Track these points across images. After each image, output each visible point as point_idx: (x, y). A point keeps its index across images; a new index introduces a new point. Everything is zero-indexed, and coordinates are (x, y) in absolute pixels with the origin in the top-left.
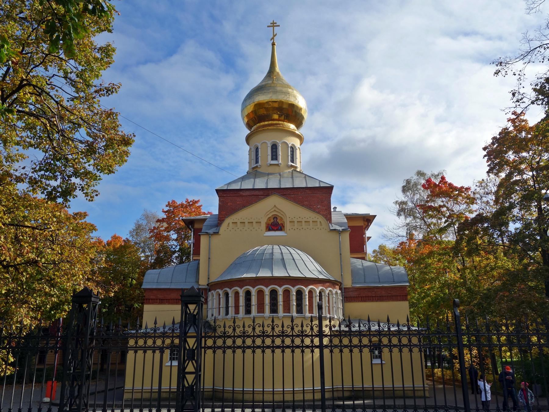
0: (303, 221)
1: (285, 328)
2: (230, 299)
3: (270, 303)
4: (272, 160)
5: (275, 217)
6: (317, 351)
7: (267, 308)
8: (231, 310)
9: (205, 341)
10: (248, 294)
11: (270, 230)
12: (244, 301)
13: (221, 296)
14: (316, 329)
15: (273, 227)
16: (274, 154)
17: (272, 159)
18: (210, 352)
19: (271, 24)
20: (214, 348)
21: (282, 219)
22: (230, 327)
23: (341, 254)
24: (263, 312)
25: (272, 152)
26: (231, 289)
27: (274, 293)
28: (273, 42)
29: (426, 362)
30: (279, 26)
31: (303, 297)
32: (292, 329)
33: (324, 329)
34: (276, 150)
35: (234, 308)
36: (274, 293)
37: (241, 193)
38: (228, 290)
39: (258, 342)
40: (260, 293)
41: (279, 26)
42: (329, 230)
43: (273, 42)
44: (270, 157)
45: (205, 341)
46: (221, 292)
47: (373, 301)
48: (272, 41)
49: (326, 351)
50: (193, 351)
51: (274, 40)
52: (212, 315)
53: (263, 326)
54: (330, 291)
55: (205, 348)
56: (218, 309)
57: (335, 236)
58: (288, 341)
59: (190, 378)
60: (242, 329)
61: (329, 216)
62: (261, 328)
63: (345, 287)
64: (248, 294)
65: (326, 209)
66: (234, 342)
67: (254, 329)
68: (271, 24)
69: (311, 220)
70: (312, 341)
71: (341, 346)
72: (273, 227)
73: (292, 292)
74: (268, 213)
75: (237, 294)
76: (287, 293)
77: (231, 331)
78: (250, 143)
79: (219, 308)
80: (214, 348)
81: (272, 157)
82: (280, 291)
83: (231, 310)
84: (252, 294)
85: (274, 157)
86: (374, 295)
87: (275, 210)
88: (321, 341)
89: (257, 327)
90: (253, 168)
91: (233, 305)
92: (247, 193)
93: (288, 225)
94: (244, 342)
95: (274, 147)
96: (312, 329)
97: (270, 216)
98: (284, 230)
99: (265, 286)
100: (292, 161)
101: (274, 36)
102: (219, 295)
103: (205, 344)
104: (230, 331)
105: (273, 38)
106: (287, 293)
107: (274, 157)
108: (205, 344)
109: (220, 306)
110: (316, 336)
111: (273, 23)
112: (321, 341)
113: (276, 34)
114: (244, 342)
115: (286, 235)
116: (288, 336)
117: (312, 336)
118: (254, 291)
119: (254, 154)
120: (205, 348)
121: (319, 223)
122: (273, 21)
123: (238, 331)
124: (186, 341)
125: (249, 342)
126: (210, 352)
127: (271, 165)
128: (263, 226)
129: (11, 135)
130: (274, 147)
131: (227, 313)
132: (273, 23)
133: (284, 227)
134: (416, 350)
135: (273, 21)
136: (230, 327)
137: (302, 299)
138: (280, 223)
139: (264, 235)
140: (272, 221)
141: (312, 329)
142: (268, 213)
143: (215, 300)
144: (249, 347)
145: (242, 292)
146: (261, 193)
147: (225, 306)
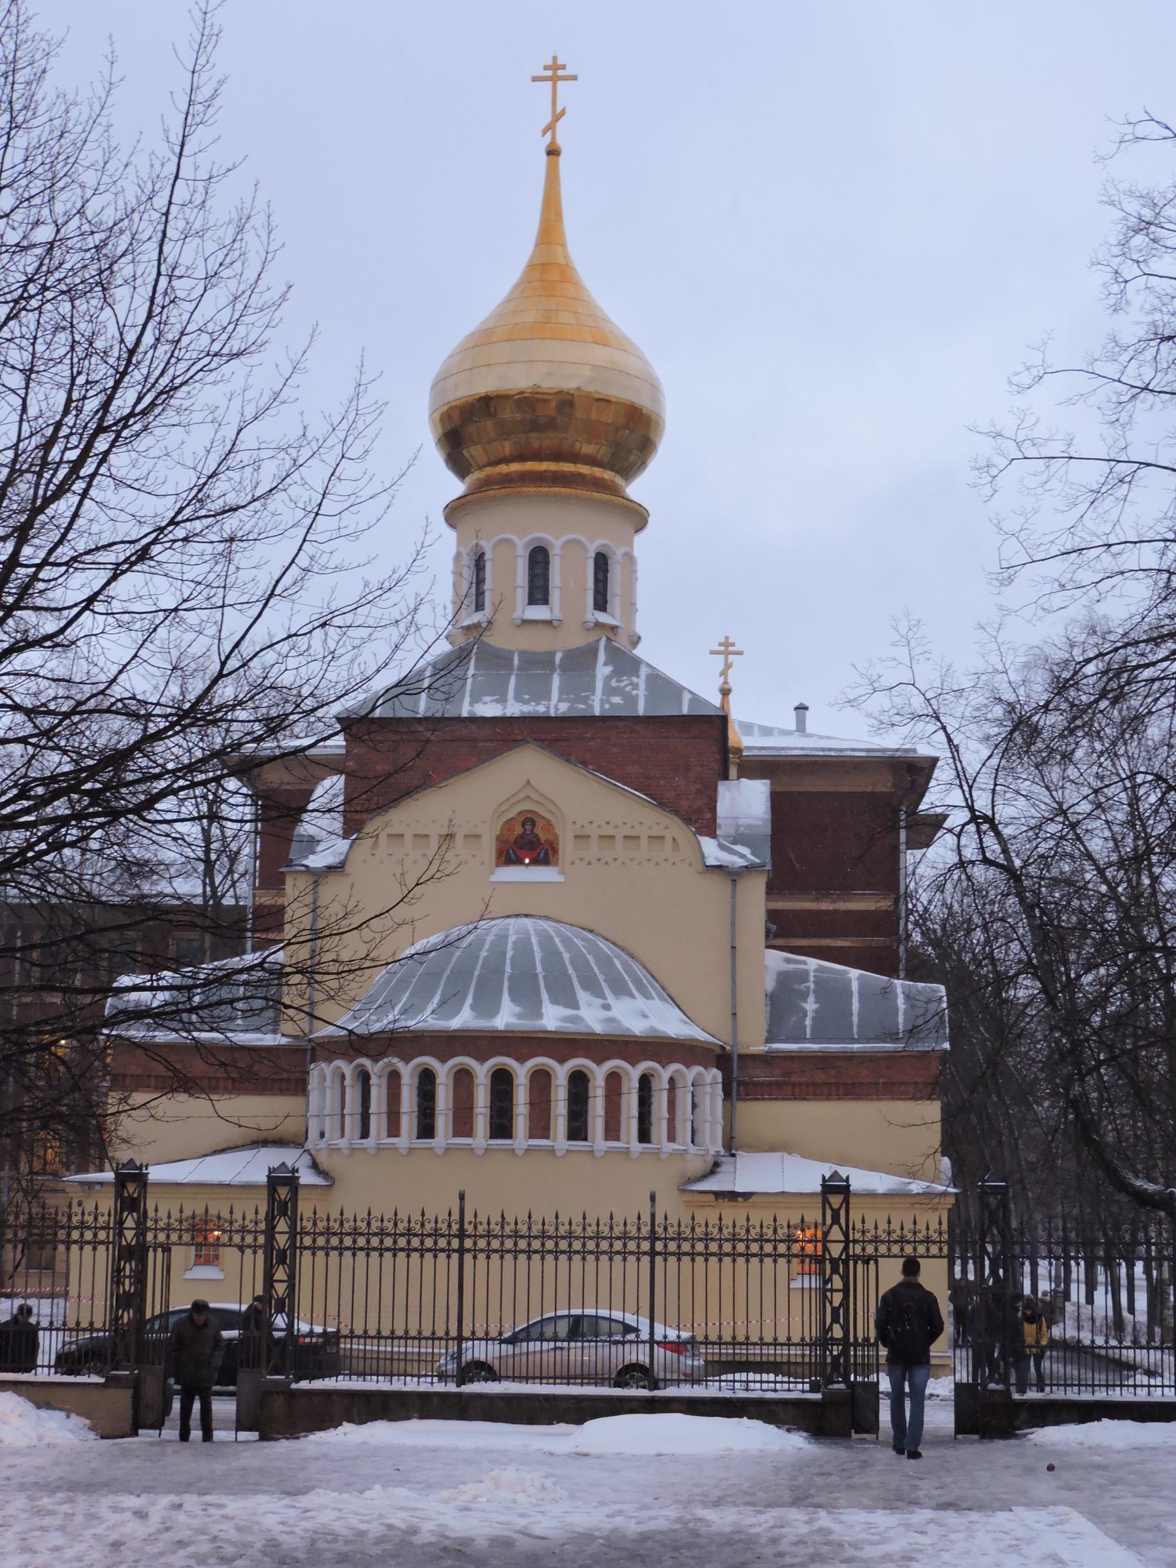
0: (619, 834)
1: (412, 1225)
2: (374, 1092)
3: (491, 1108)
5: (529, 819)
6: (455, 1256)
7: (482, 1123)
8: (378, 1123)
9: (301, 1239)
10: (427, 1079)
12: (415, 1100)
13: (347, 1082)
14: (455, 1227)
17: (532, 601)
18: (307, 1254)
19: (546, 68)
20: (314, 1249)
21: (549, 825)
22: (335, 1221)
23: (733, 948)
24: (469, 1133)
27: (502, 1081)
28: (553, 142)
29: (119, 1260)
30: (574, 78)
31: (591, 1094)
32: (423, 1225)
33: (466, 1226)
34: (546, 569)
35: (384, 1118)
36: (502, 1081)
38: (365, 1062)
39: (375, 1242)
40: (463, 1078)
41: (574, 78)
42: (700, 868)
43: (553, 142)
44: (522, 594)
45: (301, 1239)
46: (347, 1069)
47: (828, 1097)
48: (549, 134)
49: (468, 1257)
50: (284, 1251)
51: (554, 136)
52: (322, 1135)
53: (382, 1221)
54: (676, 1071)
55: (300, 1248)
56: (338, 1119)
57: (718, 887)
58: (415, 1242)
60: (352, 1223)
61: (709, 816)
62: (379, 1223)
63: (743, 1052)
64: (427, 1079)
65: (698, 792)
66: (341, 1241)
67: (369, 1224)
68: (546, 68)
69: (643, 832)
70: (449, 1243)
71: (693, 1239)
73: (557, 1078)
74: (505, 807)
75: (394, 1077)
76: (541, 1079)
77: (337, 1225)
79: (343, 1116)
80: (314, 1249)
82: (521, 1073)
83: (378, 1123)
84: (438, 1081)
85: (539, 596)
86: (833, 1081)
87: (528, 797)
88: (461, 1243)
89: (373, 1222)
91: (384, 1109)
93: (567, 848)
94: (355, 1242)
95: (539, 558)
96: (449, 1226)
97: (512, 814)
98: (556, 864)
99: (594, 1061)
100: (601, 603)
101: (557, 116)
102: (343, 1077)
103: (301, 1243)
104: (336, 1226)
105: (550, 128)
106: (541, 1079)
108: (301, 1243)
109: (345, 1111)
110: (455, 1236)
111: (555, 66)
112: (461, 1243)
113: (563, 113)
114: (543, 1245)
115: (561, 879)
116: (416, 1235)
117: (449, 1235)
118: (443, 1072)
119: (468, 574)
120: (300, 1248)
121: (668, 841)
122: (555, 58)
123: (347, 1227)
124: (273, 1238)
125: (361, 1241)
126: (307, 1254)
127: (526, 622)
128: (488, 848)
130: (540, 558)
131: (365, 1134)
132: (555, 66)
133: (555, 851)
134: (260, 1252)
135: (555, 58)
136: (335, 1221)
137: (587, 1098)
138: (543, 836)
139: (493, 878)
140: (519, 830)
141: (449, 1226)
142: (505, 807)
143: (328, 1093)
145: (408, 1072)
147: (359, 1110)
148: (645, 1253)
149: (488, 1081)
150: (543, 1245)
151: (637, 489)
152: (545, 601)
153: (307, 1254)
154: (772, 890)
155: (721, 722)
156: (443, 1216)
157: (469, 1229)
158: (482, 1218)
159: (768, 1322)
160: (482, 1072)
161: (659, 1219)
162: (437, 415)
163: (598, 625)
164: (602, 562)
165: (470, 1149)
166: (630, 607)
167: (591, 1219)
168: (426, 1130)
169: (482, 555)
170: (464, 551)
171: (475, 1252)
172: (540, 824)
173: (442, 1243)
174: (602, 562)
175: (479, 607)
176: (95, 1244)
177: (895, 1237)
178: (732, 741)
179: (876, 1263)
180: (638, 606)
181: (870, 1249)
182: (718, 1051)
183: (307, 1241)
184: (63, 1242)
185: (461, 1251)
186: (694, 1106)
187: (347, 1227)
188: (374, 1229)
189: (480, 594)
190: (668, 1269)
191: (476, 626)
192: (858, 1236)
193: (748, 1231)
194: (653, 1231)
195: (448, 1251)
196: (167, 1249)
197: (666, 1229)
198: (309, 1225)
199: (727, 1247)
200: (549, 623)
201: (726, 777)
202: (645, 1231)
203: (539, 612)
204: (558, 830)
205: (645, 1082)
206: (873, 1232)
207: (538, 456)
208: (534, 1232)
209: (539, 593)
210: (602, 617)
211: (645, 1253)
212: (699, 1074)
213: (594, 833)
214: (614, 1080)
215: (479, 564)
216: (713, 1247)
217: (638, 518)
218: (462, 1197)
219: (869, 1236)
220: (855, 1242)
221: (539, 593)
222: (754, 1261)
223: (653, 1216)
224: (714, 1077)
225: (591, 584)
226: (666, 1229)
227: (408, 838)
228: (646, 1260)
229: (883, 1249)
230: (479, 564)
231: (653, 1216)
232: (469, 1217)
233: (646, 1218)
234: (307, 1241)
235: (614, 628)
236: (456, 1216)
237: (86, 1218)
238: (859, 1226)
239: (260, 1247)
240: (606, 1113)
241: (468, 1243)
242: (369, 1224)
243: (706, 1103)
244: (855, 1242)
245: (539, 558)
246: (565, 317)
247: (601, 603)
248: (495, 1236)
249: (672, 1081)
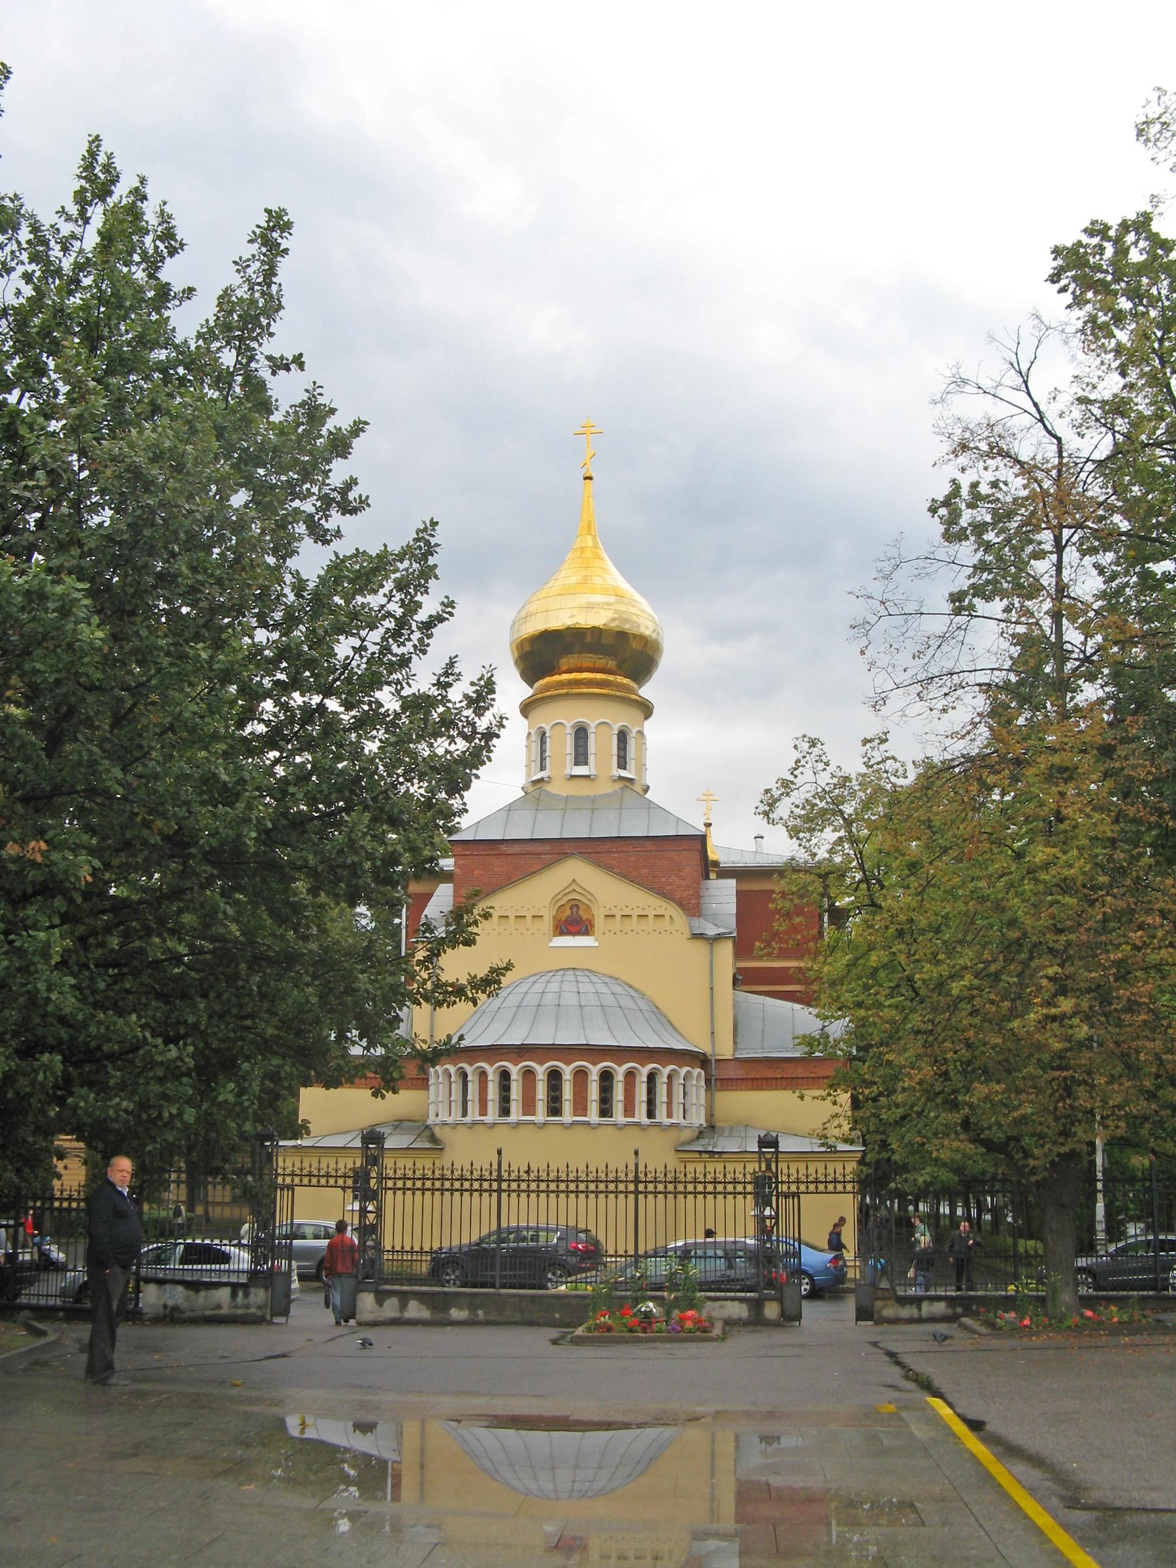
4: (576, 764)
5: (575, 905)
6: (495, 1195)
10: (505, 1075)
11: (562, 933)
14: (495, 1174)
15: (570, 927)
16: (581, 750)
18: (390, 1193)
20: (395, 1189)
25: (577, 746)
26: (471, 1065)
32: (472, 1173)
34: (586, 742)
36: (555, 1077)
37: (504, 848)
38: (465, 1065)
44: (570, 759)
46: (452, 1069)
49: (504, 1195)
57: (701, 947)
59: (371, 1217)
63: (718, 1057)
67: (433, 1172)
69: (651, 913)
72: (570, 927)
76: (581, 1075)
78: (532, 715)
80: (395, 1189)
81: (576, 758)
82: (567, 1071)
88: (500, 1186)
90: (535, 782)
92: (517, 849)
93: (599, 923)
95: (581, 733)
96: (491, 1173)
98: (593, 934)
100: (622, 764)
106: (581, 1075)
107: (581, 759)
112: (500, 1186)
114: (462, 1185)
121: (667, 917)
127: (573, 777)
128: (547, 924)
129: (77, 792)
130: (582, 734)
133: (592, 926)
134: (183, 1186)
138: (584, 918)
139: (551, 944)
140: (568, 912)
141: (491, 1173)
144: (486, 1191)
146: (546, 848)
148: (631, 1192)
149: (497, 1078)
150: (462, 1185)
151: (646, 691)
152: (586, 763)
153: (390, 1193)
154: (741, 950)
155: (702, 839)
156: (486, 1166)
157: (505, 1175)
158: (650, 1168)
159: (720, 1213)
160: (541, 1071)
161: (641, 1168)
162: (514, 645)
163: (621, 778)
164: (622, 736)
165: (587, 1123)
166: (641, 767)
167: (592, 1168)
168: (554, 1109)
169: (545, 733)
170: (533, 732)
171: (646, 1193)
172: (582, 907)
173: (486, 1185)
174: (622, 736)
175: (543, 768)
176: (745, 1194)
177: (811, 1179)
178: (712, 856)
179: (799, 1198)
180: (648, 766)
181: (793, 1188)
182: (702, 1057)
183: (390, 1184)
184: (174, 1182)
185: (499, 1191)
186: (685, 1094)
187: (533, 1176)
188: (437, 1175)
189: (543, 759)
190: (648, 1203)
191: (541, 780)
192: (785, 1178)
193: (705, 1175)
194: (636, 1176)
195: (490, 1191)
196: (291, 1188)
197: (646, 1175)
198: (391, 1173)
199: (670, 1187)
200: (588, 777)
201: (708, 878)
202: (631, 1177)
203: (581, 770)
204: (595, 911)
205: (651, 1078)
206: (343, 1170)
207: (580, 670)
208: (591, 1177)
209: (581, 757)
210: (624, 773)
211: (631, 1192)
212: (688, 1072)
213: (618, 913)
214: (630, 1075)
215: (543, 736)
216: (680, 1188)
217: (646, 709)
218: (499, 1152)
219: (792, 1179)
220: (782, 1182)
221: (581, 757)
222: (710, 1197)
223: (637, 1165)
224: (699, 1074)
225: (615, 751)
226: (646, 1175)
227: (529, 918)
228: (631, 1197)
229: (803, 1187)
230: (543, 736)
231: (637, 1165)
232: (504, 1167)
233: (632, 1167)
234: (390, 1184)
235: (631, 780)
236: (495, 1166)
237: (445, 1172)
238: (785, 1171)
239: (183, 1182)
240: (625, 1099)
241: (504, 1186)
242: (433, 1172)
243: (693, 1092)
244: (782, 1182)
245: (581, 733)
246: (597, 580)
247: (622, 764)
248: (660, 1182)
249: (670, 1077)
